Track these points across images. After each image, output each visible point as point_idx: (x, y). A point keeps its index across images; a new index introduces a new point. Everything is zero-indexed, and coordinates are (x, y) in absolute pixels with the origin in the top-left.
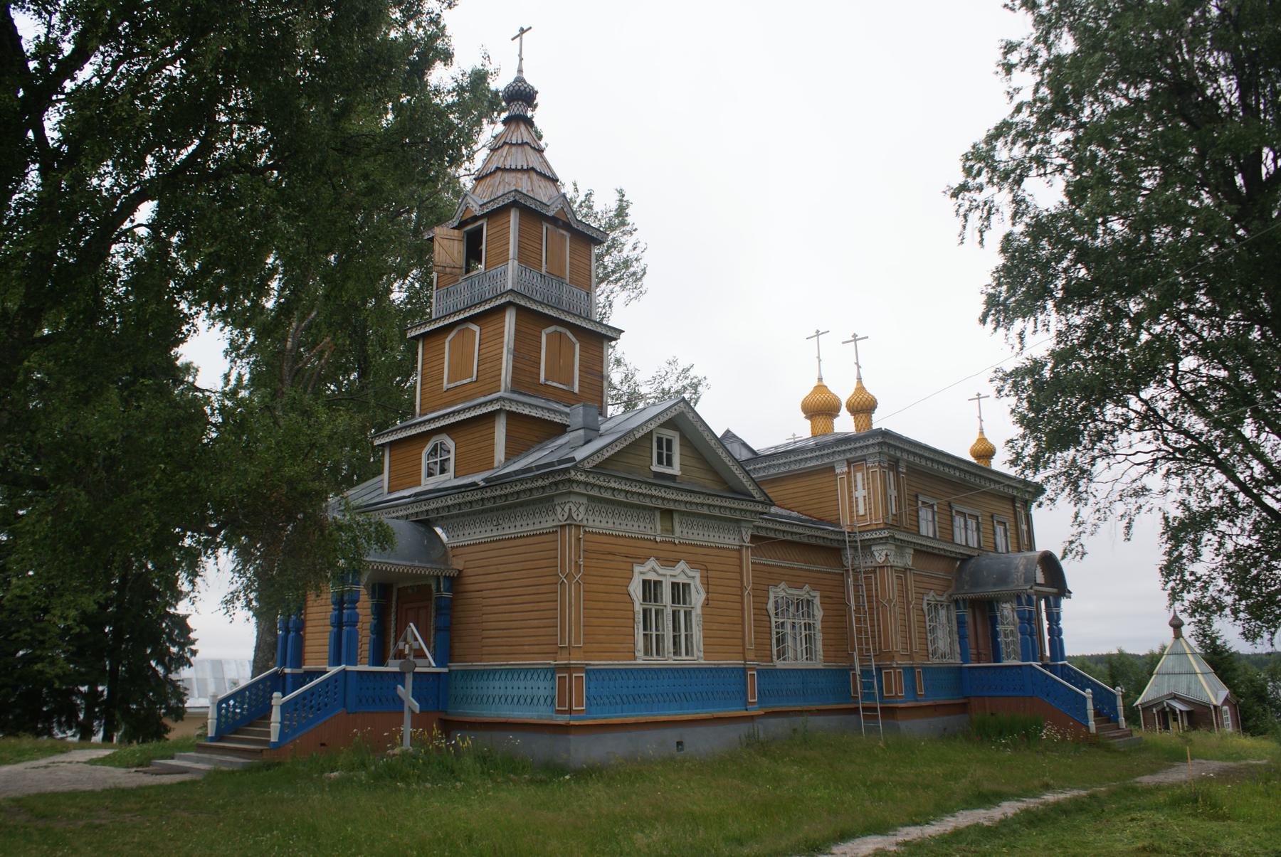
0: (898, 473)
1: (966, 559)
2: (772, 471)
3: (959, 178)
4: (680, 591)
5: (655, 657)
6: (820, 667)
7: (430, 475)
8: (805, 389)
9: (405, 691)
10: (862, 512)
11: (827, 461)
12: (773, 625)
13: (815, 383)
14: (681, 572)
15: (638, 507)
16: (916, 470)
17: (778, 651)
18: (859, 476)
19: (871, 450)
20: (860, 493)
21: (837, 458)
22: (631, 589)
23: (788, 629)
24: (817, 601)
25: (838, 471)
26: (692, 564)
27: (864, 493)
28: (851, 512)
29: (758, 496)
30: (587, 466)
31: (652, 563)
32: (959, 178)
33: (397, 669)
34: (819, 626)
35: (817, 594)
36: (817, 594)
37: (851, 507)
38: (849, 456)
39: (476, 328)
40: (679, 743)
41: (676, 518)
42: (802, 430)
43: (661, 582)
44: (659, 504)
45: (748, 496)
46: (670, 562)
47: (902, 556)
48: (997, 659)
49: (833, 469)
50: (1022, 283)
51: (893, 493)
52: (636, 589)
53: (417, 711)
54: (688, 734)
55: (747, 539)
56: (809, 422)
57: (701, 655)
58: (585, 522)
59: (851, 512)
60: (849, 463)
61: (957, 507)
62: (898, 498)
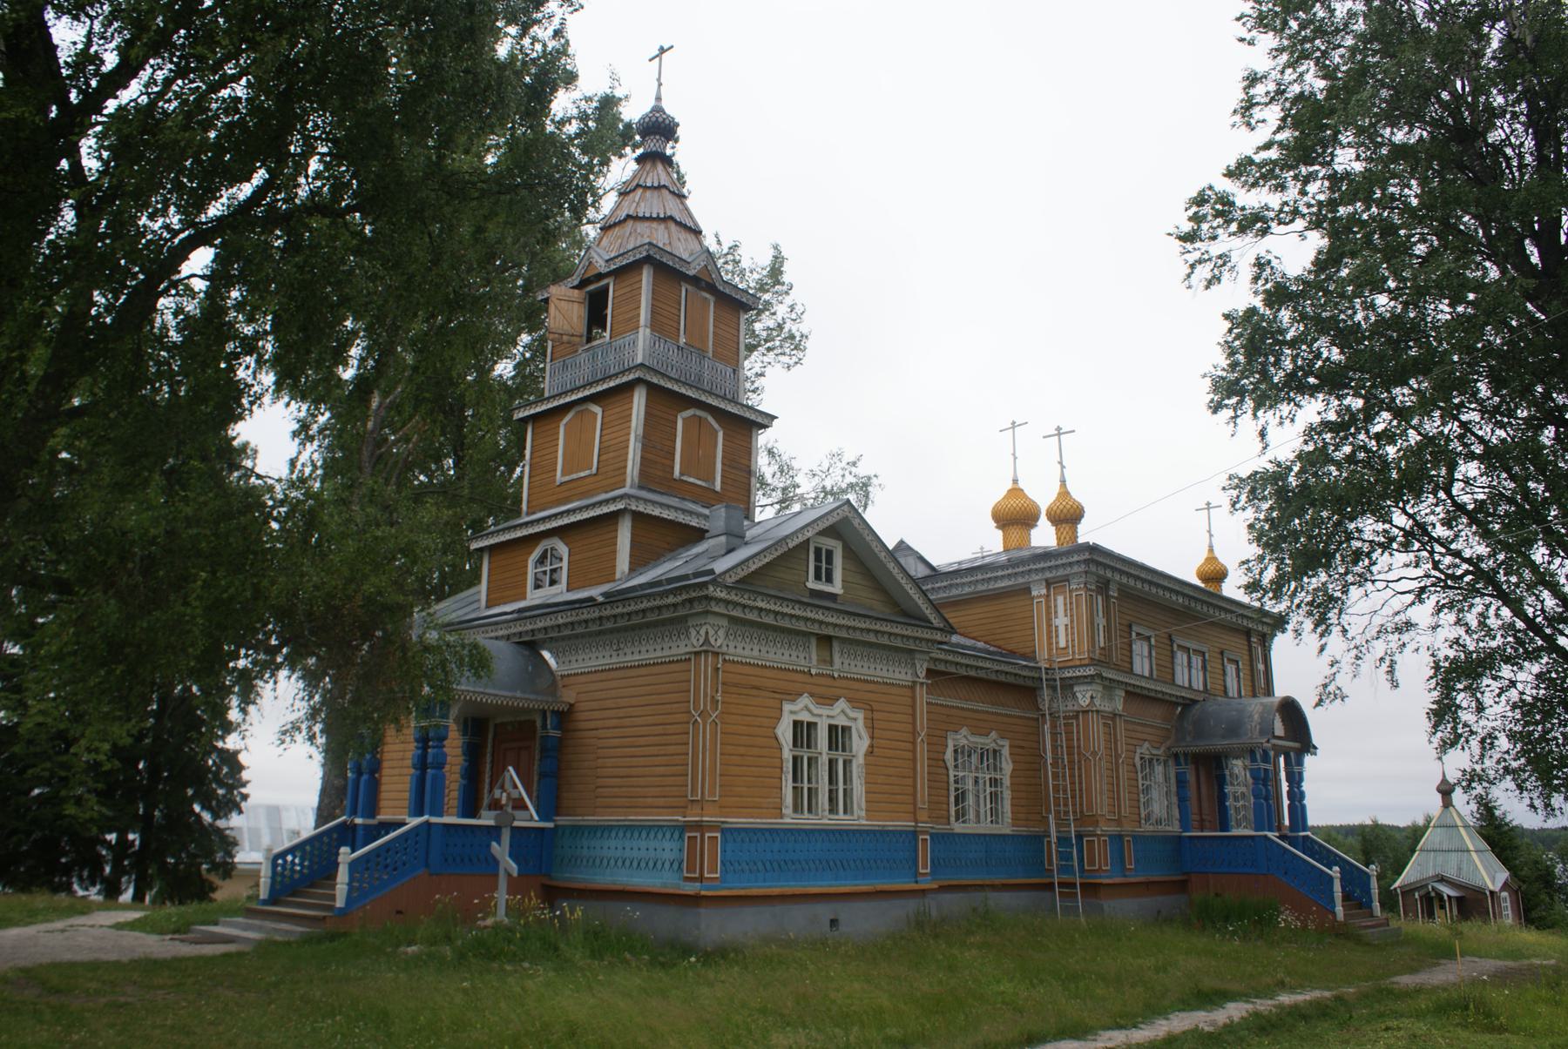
0: (1108, 597)
4: (838, 736)
7: (537, 587)
8: (997, 492)
9: (500, 850)
10: (1062, 644)
11: (1021, 580)
13: (1009, 486)
14: (840, 713)
18: (1060, 599)
19: (1076, 569)
20: (1061, 621)
22: (779, 732)
24: (1006, 752)
25: (1034, 593)
26: (854, 702)
27: (1066, 620)
28: (1050, 644)
29: (936, 622)
31: (805, 700)
34: (1007, 782)
35: (1006, 743)
36: (1006, 743)
37: (1050, 638)
38: (1048, 575)
39: (597, 410)
40: (834, 923)
41: (836, 646)
44: (816, 629)
45: (923, 621)
47: (1111, 699)
51: (1101, 621)
52: (785, 732)
53: (515, 874)
54: (844, 911)
55: (922, 673)
56: (1000, 533)
57: (863, 814)
59: (1050, 644)
60: (1048, 583)
61: (1179, 641)
62: (1108, 629)
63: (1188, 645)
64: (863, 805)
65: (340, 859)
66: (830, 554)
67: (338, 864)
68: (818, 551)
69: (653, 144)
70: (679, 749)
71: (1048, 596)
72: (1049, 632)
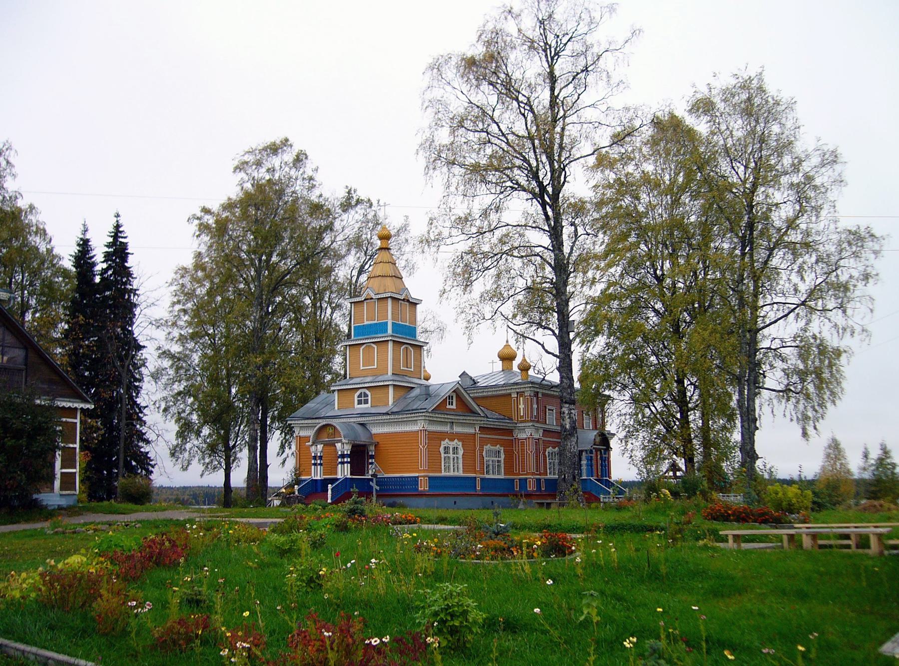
0: (538, 398)
4: (455, 450)
20: (522, 406)
24: (460, 447)
46: (452, 440)
49: (510, 394)
51: (535, 406)
52: (442, 450)
60: (517, 393)
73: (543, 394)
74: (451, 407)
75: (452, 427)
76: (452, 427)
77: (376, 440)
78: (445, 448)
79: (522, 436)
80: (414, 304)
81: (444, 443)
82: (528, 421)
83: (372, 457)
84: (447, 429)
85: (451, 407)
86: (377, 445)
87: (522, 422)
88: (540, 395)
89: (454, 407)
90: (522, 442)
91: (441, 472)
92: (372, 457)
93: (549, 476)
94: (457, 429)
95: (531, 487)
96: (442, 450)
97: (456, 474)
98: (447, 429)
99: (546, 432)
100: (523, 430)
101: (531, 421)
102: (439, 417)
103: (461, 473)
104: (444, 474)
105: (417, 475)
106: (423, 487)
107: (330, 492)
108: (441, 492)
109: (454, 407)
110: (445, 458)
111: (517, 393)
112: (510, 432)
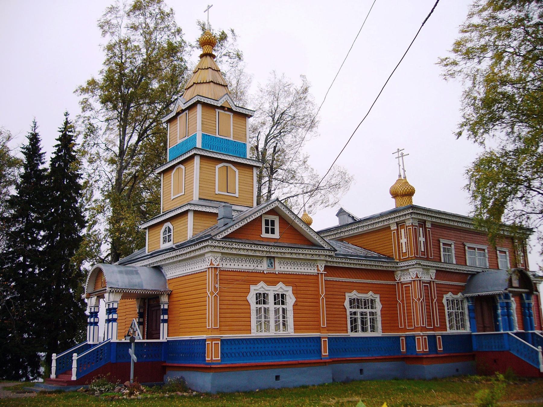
0: (426, 228)
1: (473, 275)
2: (360, 230)
3: (85, 85)
4: (280, 299)
5: (282, 332)
6: (380, 336)
7: (165, 241)
8: (392, 181)
9: (131, 351)
10: (404, 251)
11: (386, 223)
12: (348, 313)
13: (397, 178)
14: (281, 288)
15: (180, 261)
16: (437, 226)
17: (449, 321)
18: (403, 230)
19: (408, 217)
20: (403, 240)
21: (391, 222)
22: (249, 298)
23: (359, 316)
24: (378, 300)
25: (392, 229)
26: (287, 283)
27: (405, 240)
28: (399, 251)
29: (326, 247)
30: (218, 238)
31: (262, 284)
32: (85, 85)
33: (129, 341)
34: (379, 313)
35: (378, 296)
36: (378, 296)
37: (399, 248)
38: (396, 220)
39: (182, 167)
40: (361, 371)
41: (277, 261)
42: (391, 204)
43: (267, 295)
44: (264, 254)
45: (322, 248)
46: (274, 283)
47: (428, 273)
48: (498, 330)
49: (389, 227)
50: (488, 111)
51: (422, 239)
52: (251, 298)
53: (136, 361)
54: (365, 365)
55: (322, 269)
56: (394, 200)
57: (293, 330)
58: (220, 266)
59: (399, 251)
60: (397, 224)
61: (468, 245)
62: (426, 243)
63: (475, 246)
64: (293, 327)
65: (53, 358)
66: (273, 223)
67: (72, 360)
68: (267, 222)
69: (208, 49)
70: (223, 307)
71: (398, 229)
72: (399, 246)
73: (434, 225)
74: (270, 236)
75: (271, 264)
76: (271, 264)
77: (169, 287)
78: (258, 296)
79: (406, 278)
80: (244, 116)
81: (254, 290)
82: (412, 259)
83: (165, 312)
84: (264, 266)
85: (270, 236)
86: (170, 295)
87: (405, 260)
88: (428, 225)
89: (277, 235)
90: (406, 286)
91: (159, 338)
92: (165, 312)
93: (449, 331)
94: (279, 267)
95: (421, 348)
96: (251, 298)
97: (282, 333)
98: (264, 266)
99: (440, 273)
100: (405, 270)
101: (416, 258)
102: (236, 247)
103: (290, 332)
104: (255, 333)
105: (204, 337)
106: (213, 355)
107: (74, 365)
108: (253, 362)
109: (277, 235)
110: (258, 311)
111: (397, 224)
112: (390, 274)
